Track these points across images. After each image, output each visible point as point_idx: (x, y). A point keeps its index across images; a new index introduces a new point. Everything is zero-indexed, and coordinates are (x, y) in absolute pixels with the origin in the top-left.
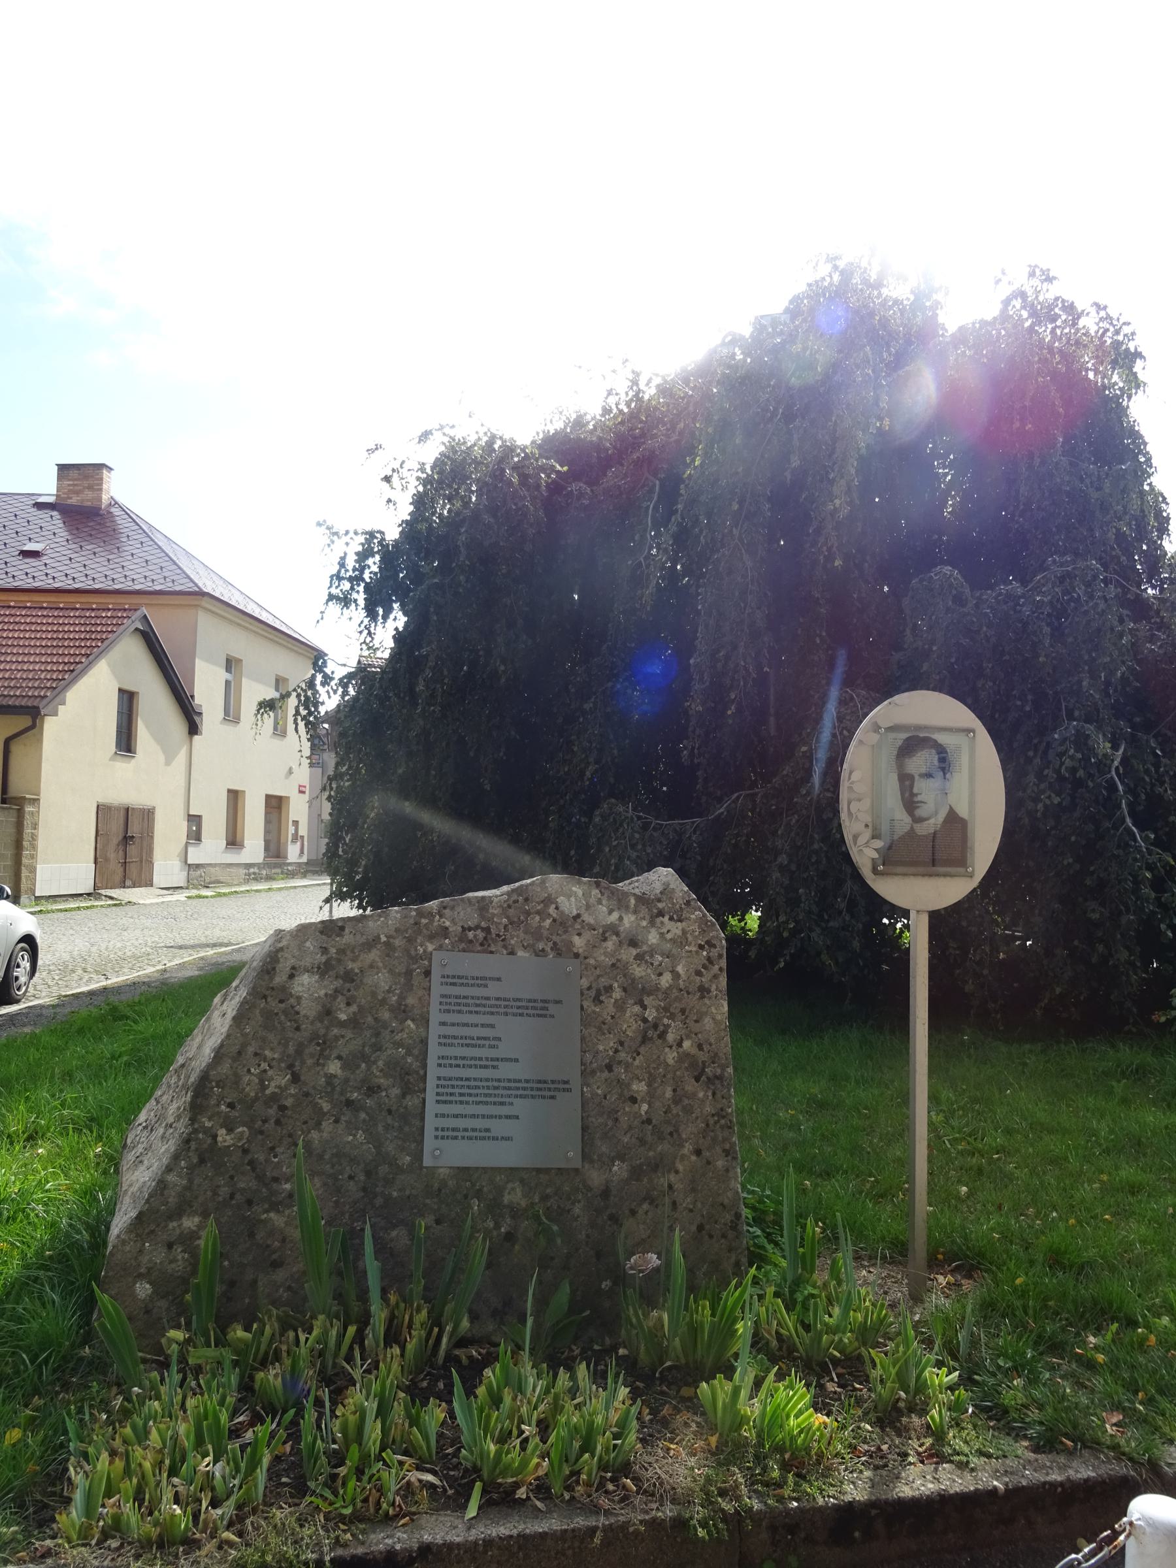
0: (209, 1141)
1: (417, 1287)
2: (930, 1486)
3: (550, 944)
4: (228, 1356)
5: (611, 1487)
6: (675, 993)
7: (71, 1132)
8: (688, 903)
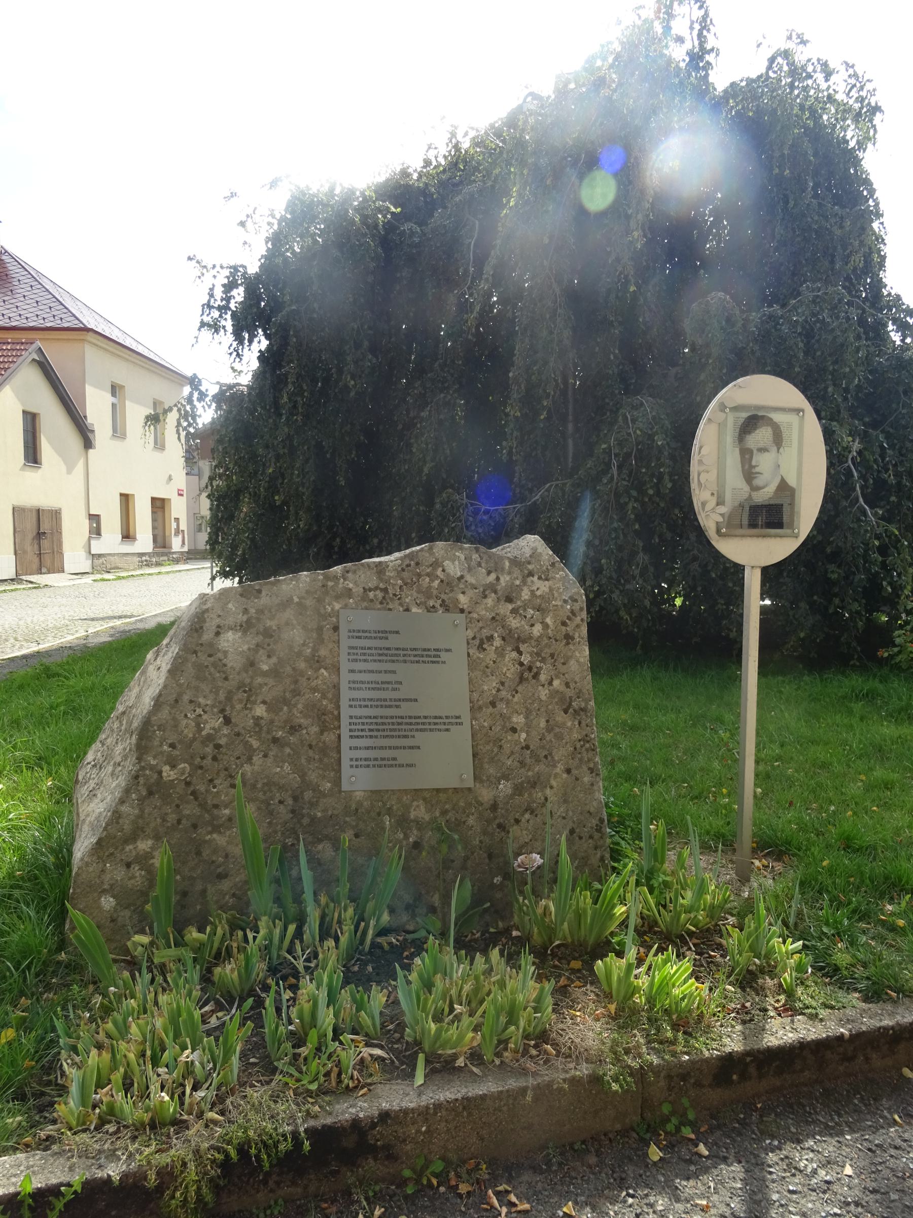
0: (155, 776)
1: (343, 889)
2: (791, 1035)
3: (439, 602)
4: (189, 955)
5: (534, 1052)
6: (545, 641)
7: (25, 770)
8: (553, 565)
